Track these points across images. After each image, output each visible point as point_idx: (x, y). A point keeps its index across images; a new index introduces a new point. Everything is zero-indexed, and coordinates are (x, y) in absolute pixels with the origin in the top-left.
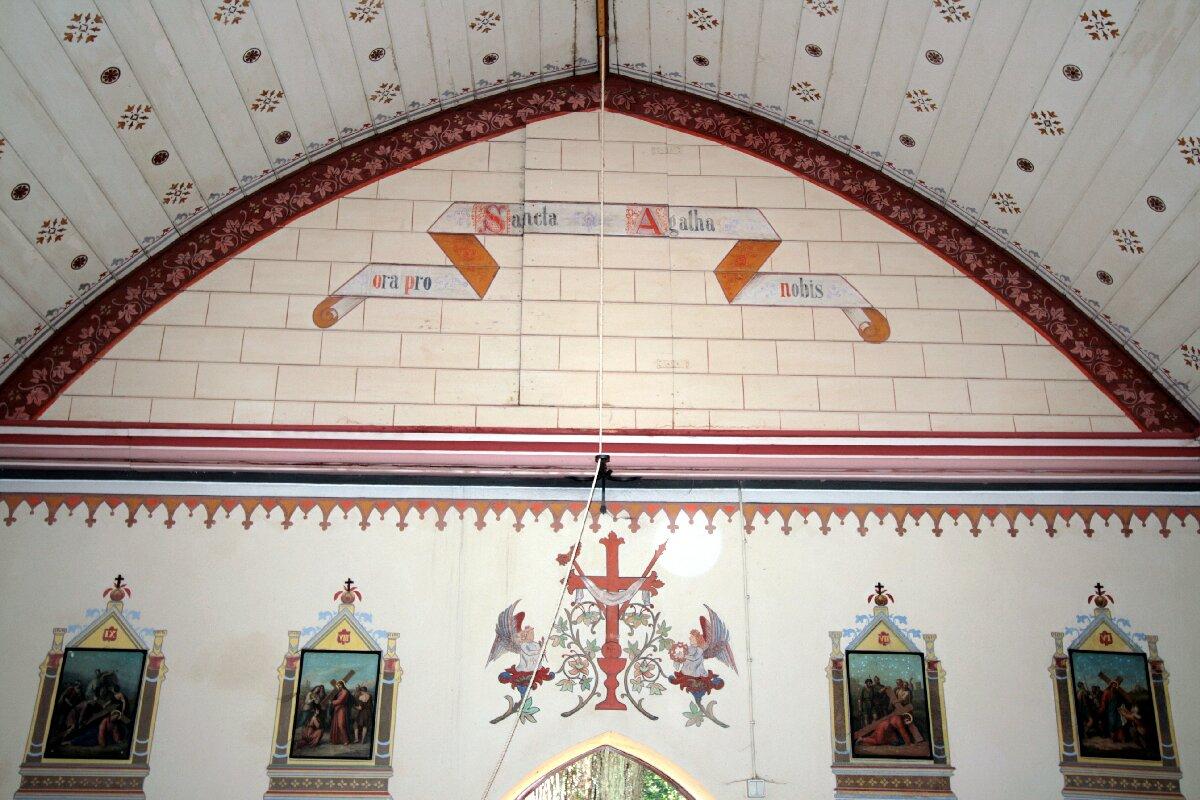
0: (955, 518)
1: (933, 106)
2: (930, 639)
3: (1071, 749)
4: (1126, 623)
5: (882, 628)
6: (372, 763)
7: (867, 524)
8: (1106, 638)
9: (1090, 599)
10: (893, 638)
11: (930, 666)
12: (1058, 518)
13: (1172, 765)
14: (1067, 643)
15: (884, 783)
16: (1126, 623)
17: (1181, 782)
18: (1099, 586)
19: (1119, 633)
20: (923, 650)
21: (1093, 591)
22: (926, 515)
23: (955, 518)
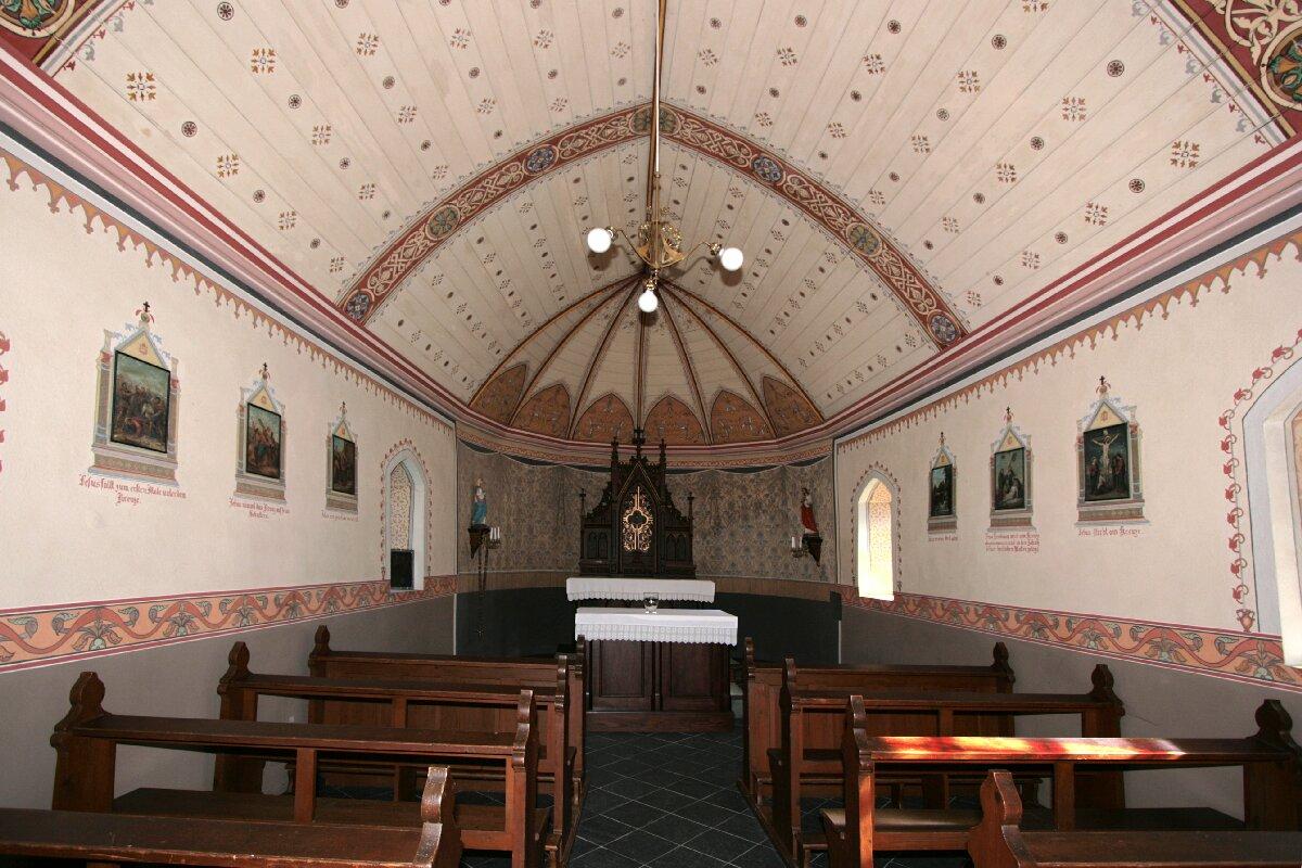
0: (209, 287)
1: (362, 197)
2: (175, 361)
3: (104, 432)
4: (159, 340)
5: (263, 393)
6: (165, 456)
7: (153, 260)
8: (264, 400)
9: (138, 312)
10: (150, 350)
11: (170, 382)
12: (223, 296)
13: (173, 459)
14: (115, 344)
15: (144, 468)
16: (159, 340)
17: (176, 472)
18: (146, 305)
19: (152, 345)
20: (280, 413)
21: (262, 368)
22: (213, 288)
23: (209, 287)
